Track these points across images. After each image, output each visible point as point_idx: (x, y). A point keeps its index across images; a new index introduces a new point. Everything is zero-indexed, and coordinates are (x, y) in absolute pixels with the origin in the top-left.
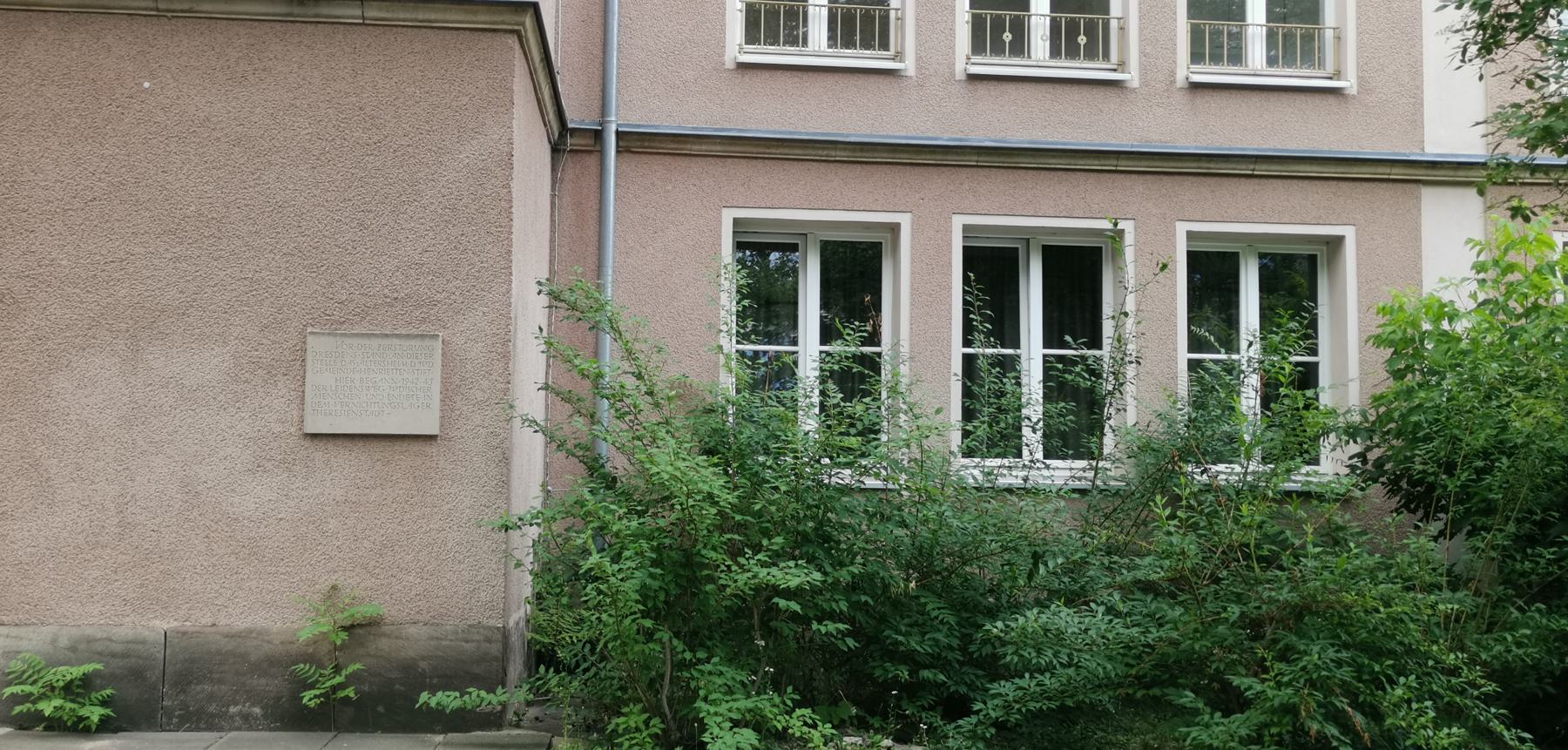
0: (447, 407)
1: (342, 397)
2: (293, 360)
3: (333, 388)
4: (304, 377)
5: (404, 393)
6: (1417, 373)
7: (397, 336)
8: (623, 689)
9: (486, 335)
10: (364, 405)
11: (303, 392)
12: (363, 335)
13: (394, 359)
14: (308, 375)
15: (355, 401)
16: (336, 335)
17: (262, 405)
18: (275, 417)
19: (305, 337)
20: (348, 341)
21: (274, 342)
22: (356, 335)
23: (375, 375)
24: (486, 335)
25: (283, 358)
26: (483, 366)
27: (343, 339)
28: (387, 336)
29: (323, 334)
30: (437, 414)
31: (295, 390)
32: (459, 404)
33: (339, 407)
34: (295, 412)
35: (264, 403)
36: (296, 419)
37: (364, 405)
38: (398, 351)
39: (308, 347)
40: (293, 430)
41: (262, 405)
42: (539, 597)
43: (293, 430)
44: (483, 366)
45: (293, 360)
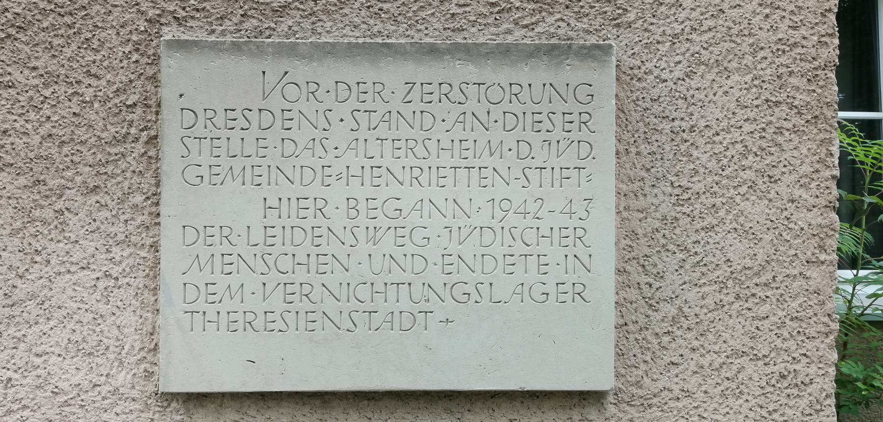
0: (632, 294)
1: (286, 263)
2: (117, 141)
3: (258, 235)
4: (155, 199)
5: (498, 250)
6: (830, 118)
7: (469, 52)
8: (129, 188)
9: (756, 48)
10: (364, 292)
11: (155, 247)
12: (352, 51)
13: (458, 133)
14: (168, 192)
15: (331, 281)
16: (259, 51)
17: (18, 295)
18: (62, 335)
19: (156, 60)
20: (301, 71)
21: (49, 79)
22: (331, 51)
23: (395, 189)
24: (756, 48)
25: (82, 133)
26: (746, 152)
27: (286, 64)
28: (433, 51)
29: (216, 47)
30: (610, 317)
31: (126, 242)
32: (672, 282)
33: (276, 302)
34: (129, 318)
35: (23, 288)
36: (133, 340)
37: (364, 292)
38: (470, 106)
39: (167, 94)
40: (122, 378)
41: (18, 295)
42: (368, 400)
43: (122, 378)
44: (746, 152)
45: (117, 141)
